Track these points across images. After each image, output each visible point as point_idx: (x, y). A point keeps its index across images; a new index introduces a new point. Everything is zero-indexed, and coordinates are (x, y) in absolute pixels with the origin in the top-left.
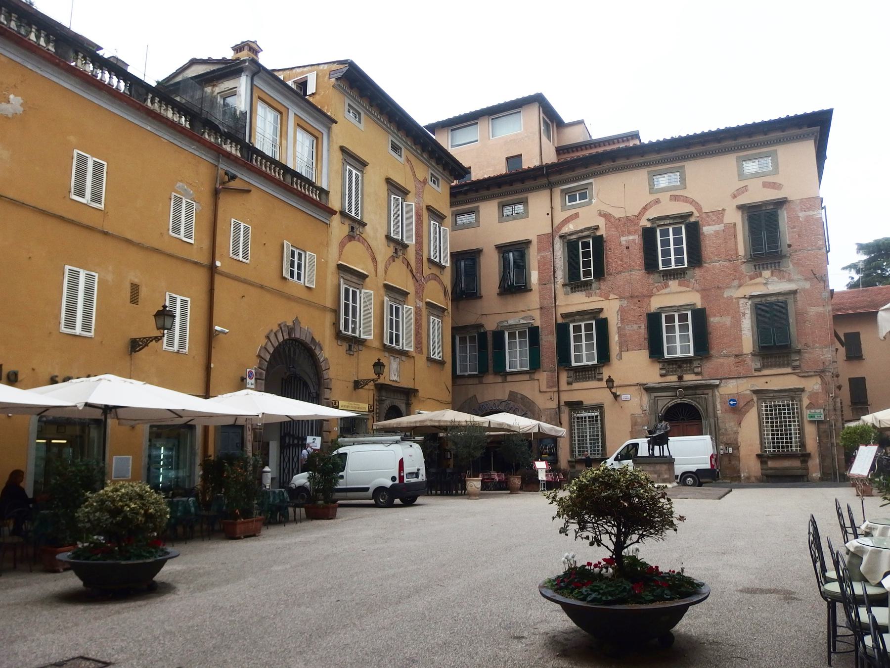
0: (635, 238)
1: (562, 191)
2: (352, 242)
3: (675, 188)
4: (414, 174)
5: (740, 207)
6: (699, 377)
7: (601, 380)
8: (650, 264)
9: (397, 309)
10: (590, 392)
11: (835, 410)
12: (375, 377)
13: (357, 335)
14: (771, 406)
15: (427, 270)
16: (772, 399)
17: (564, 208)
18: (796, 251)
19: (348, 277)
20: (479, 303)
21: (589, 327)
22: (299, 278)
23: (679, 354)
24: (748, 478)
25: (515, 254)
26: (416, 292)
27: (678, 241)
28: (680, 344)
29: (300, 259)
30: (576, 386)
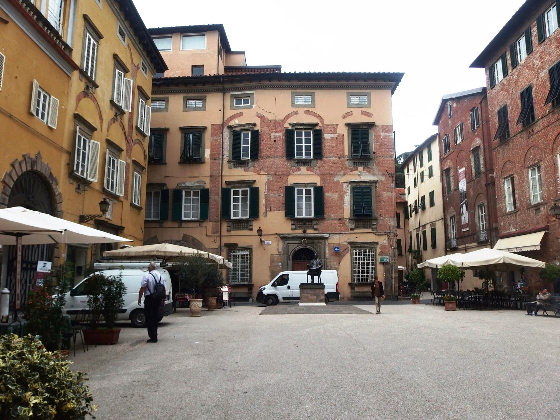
0: (280, 135)
1: (232, 96)
2: (86, 99)
3: (308, 106)
4: (132, 59)
5: (347, 125)
6: (316, 232)
7: (251, 230)
8: (289, 154)
9: (114, 161)
10: (242, 238)
11: (394, 256)
12: (101, 213)
13: (85, 177)
14: (359, 253)
15: (135, 136)
16: (360, 248)
17: (232, 108)
18: (378, 157)
19: (83, 127)
20: (163, 168)
21: (245, 193)
22: (43, 117)
23: (304, 216)
24: (343, 298)
25: (194, 136)
26: (127, 151)
27: (308, 141)
28: (305, 208)
29: (45, 100)
30: (233, 233)
